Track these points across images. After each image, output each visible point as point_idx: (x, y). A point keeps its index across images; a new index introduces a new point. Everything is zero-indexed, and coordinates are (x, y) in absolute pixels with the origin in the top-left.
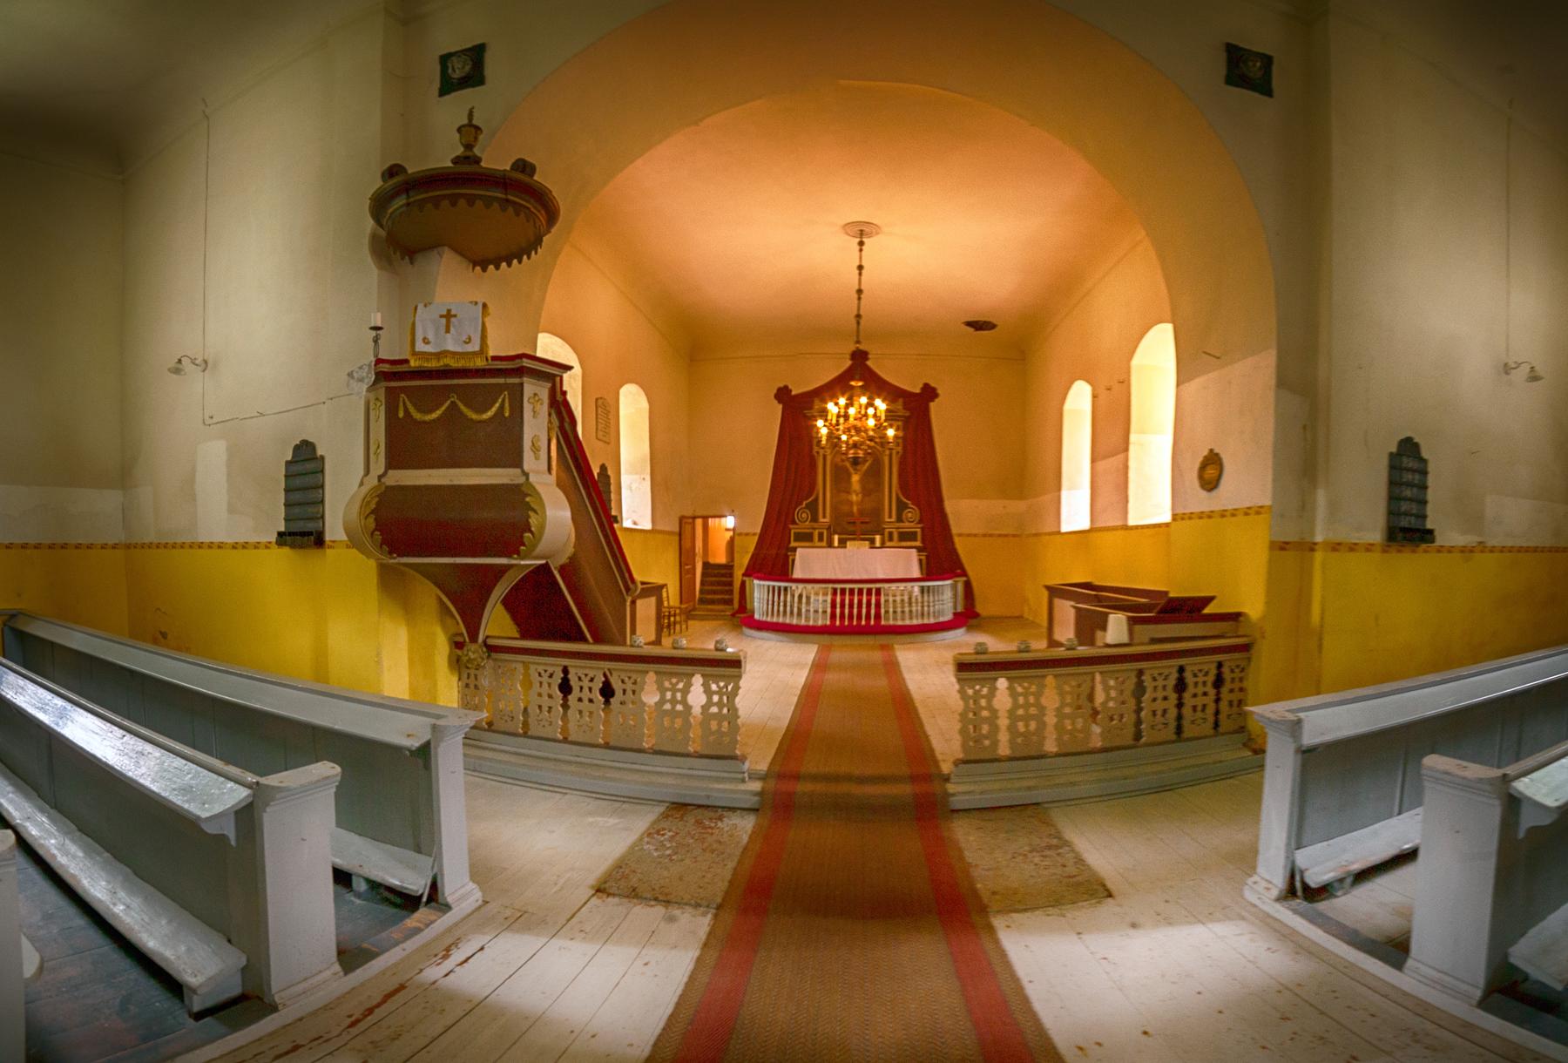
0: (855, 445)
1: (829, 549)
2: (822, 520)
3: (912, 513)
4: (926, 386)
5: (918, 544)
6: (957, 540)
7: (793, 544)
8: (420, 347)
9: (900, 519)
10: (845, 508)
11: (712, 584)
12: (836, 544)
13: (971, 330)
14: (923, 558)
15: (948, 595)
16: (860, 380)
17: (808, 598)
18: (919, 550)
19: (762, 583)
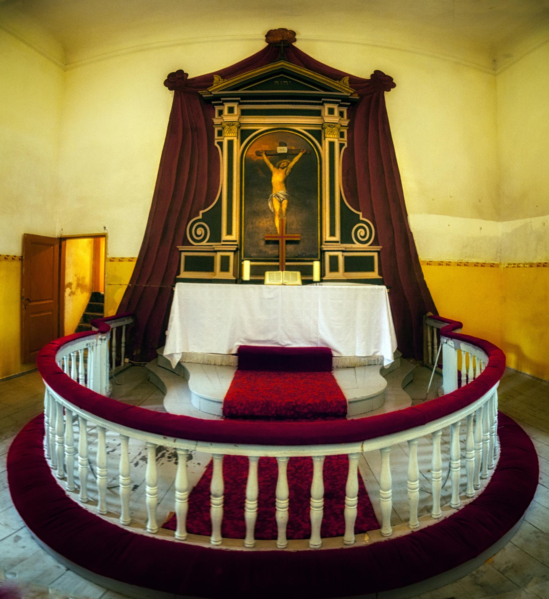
2: (225, 237)
6: (425, 269)
9: (346, 238)
12: (246, 276)
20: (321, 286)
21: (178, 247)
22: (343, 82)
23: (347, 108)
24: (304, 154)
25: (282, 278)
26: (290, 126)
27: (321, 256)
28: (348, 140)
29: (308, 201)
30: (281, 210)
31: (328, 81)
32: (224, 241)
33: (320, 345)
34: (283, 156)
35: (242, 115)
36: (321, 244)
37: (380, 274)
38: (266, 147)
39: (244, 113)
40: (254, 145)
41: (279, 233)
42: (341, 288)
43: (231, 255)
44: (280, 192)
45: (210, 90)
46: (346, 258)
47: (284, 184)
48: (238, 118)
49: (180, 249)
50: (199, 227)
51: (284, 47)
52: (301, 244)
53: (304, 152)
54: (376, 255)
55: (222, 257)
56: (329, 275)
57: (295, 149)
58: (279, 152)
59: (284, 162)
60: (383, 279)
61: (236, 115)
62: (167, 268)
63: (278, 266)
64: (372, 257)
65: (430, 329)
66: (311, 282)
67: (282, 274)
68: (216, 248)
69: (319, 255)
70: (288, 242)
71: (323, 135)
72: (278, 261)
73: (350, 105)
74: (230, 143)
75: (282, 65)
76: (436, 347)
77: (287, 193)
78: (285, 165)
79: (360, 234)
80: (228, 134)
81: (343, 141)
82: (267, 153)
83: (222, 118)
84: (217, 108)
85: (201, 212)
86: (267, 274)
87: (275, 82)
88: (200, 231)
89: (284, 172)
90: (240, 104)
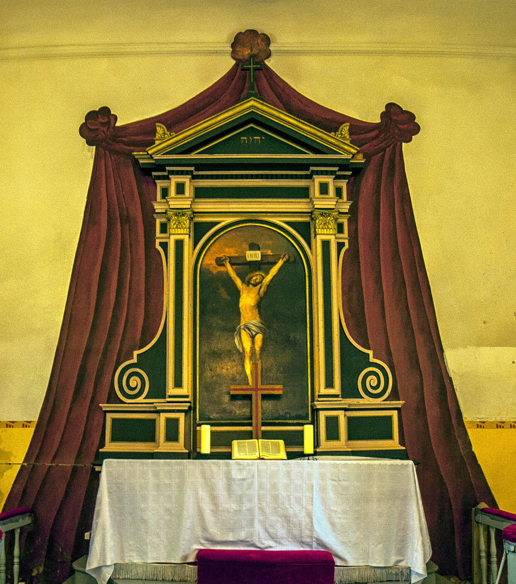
2: (171, 390)
6: (472, 433)
12: (206, 447)
20: (315, 461)
21: (100, 405)
22: (341, 134)
23: (347, 181)
24: (285, 262)
25: (258, 451)
26: (264, 216)
27: (313, 418)
28: (349, 236)
29: (292, 336)
30: (253, 349)
31: (319, 134)
32: (170, 397)
33: (315, 548)
34: (255, 266)
35: (196, 198)
36: (313, 400)
37: (402, 442)
38: (231, 252)
39: (200, 193)
40: (213, 249)
41: (250, 384)
42: (345, 464)
43: (181, 417)
44: (251, 322)
45: (150, 152)
46: (350, 421)
47: (257, 310)
48: (190, 203)
49: (104, 409)
50: (131, 377)
51: (256, 69)
52: (283, 400)
53: (285, 259)
54: (395, 414)
55: (168, 420)
57: (271, 254)
58: (249, 259)
59: (257, 275)
60: (406, 450)
61: (188, 198)
62: (84, 435)
63: (251, 432)
64: (390, 418)
65: (484, 530)
66: (301, 455)
68: (158, 406)
69: (310, 416)
70: (265, 397)
71: (312, 230)
72: (250, 424)
73: (352, 174)
74: (179, 244)
75: (252, 106)
76: (494, 559)
77: (262, 323)
78: (258, 281)
79: (371, 386)
80: (176, 230)
81: (341, 238)
82: (233, 262)
83: (167, 202)
84: (160, 184)
85: (136, 353)
86: (235, 443)
87: (242, 138)
88: (134, 382)
89: (257, 292)
90: (194, 177)
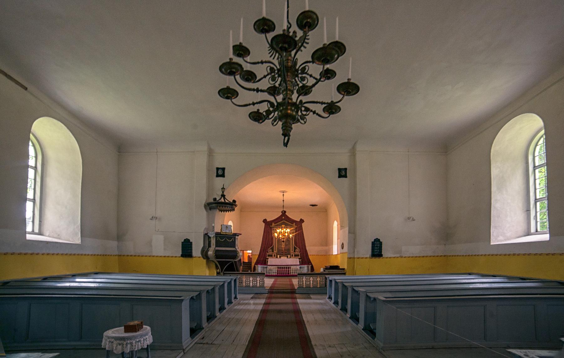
0: (283, 238)
1: (277, 259)
2: (274, 251)
3: (298, 250)
4: (301, 219)
5: (299, 257)
6: (309, 256)
7: (267, 257)
8: (223, 231)
9: (295, 251)
10: (281, 249)
11: (245, 267)
12: (278, 257)
13: (311, 206)
14: (301, 261)
15: (306, 268)
16: (284, 225)
17: (272, 270)
18: (299, 259)
19: (261, 266)
37: (300, 257)
56: (291, 257)
66: (288, 258)
67: (284, 257)
84: (273, 229)
88: (270, 250)
